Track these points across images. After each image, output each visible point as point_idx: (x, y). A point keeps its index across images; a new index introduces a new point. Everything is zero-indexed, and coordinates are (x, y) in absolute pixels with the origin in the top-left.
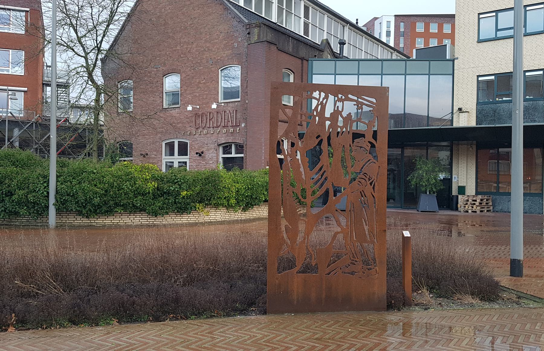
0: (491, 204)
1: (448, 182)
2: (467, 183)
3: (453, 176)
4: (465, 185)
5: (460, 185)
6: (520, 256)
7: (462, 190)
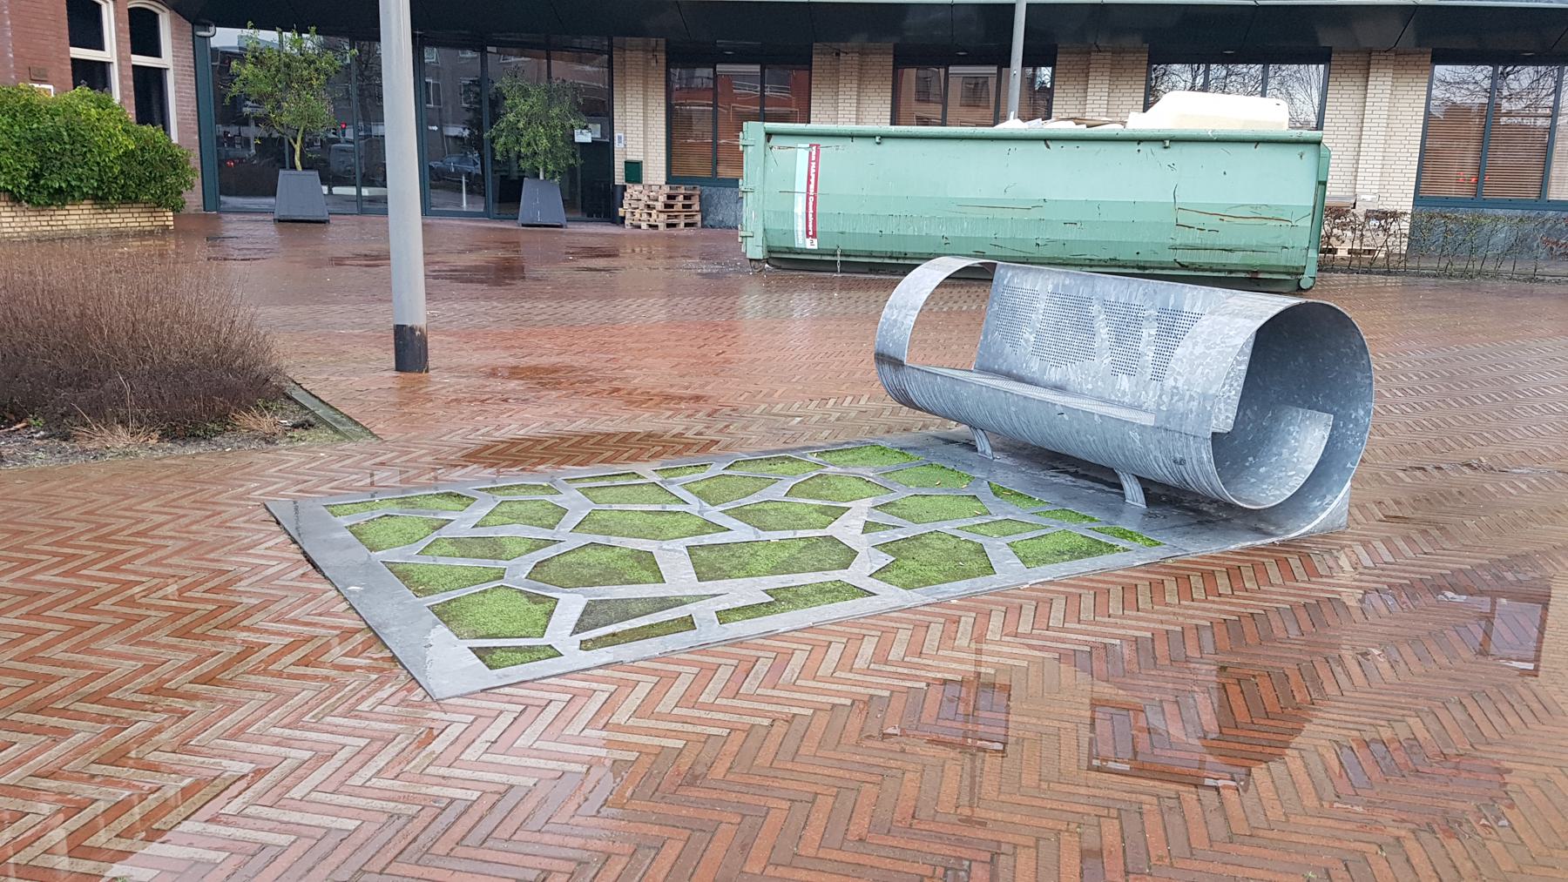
0: (696, 207)
1: (603, 150)
2: (645, 153)
3: (616, 135)
4: (640, 158)
5: (630, 158)
6: (416, 311)
7: (634, 171)
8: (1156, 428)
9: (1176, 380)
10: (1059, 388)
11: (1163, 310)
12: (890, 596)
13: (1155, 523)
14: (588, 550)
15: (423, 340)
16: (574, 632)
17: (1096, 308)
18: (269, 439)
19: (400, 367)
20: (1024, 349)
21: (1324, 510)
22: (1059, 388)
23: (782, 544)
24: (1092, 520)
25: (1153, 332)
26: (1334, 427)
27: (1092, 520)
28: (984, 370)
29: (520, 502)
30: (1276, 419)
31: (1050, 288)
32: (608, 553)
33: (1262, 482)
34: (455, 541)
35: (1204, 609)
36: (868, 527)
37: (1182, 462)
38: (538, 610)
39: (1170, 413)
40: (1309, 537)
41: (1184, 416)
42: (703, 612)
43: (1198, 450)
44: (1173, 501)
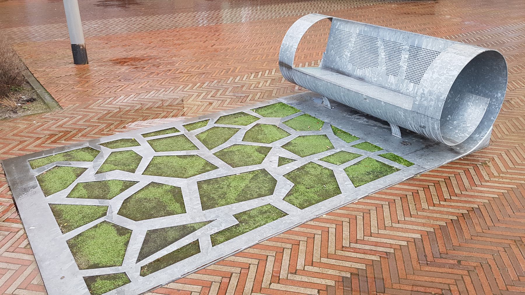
8: (412, 112)
9: (423, 90)
10: (361, 79)
11: (412, 46)
12: (296, 216)
13: (407, 148)
14: (150, 188)
15: (84, 50)
16: (139, 260)
17: (379, 43)
18: (14, 111)
19: (76, 62)
20: (345, 59)
21: (481, 139)
22: (361, 79)
23: (242, 177)
24: (379, 149)
25: (407, 56)
26: (490, 105)
27: (379, 149)
28: (326, 68)
29: (121, 152)
30: (462, 99)
31: (358, 31)
32: (160, 190)
33: (455, 128)
34: (87, 185)
35: (441, 212)
36: (282, 161)
37: (424, 127)
38: (122, 239)
39: (420, 106)
40: (474, 151)
41: (426, 108)
42: (203, 236)
43: (433, 124)
44: (418, 140)
